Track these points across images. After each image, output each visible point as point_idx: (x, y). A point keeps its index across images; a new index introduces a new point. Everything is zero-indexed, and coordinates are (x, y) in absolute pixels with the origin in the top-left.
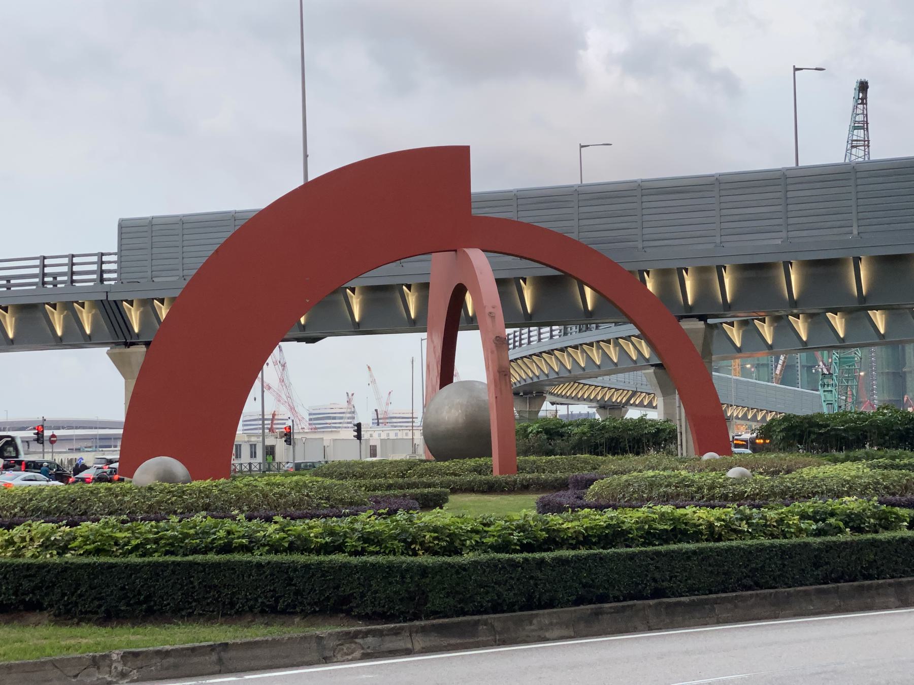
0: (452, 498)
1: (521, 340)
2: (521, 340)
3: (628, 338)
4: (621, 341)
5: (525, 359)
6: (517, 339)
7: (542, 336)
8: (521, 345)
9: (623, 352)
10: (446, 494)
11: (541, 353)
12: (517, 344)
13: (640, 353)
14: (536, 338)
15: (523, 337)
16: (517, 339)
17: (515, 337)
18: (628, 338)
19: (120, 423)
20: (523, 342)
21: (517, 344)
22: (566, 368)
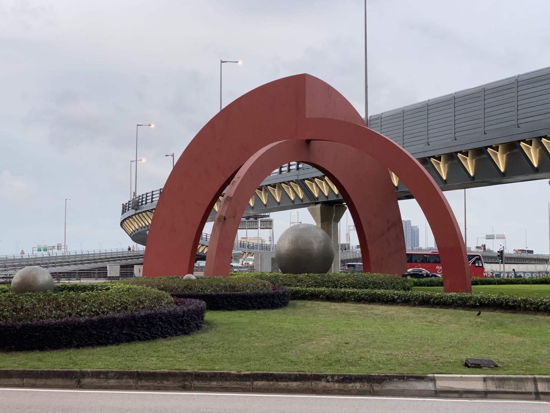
0: (209, 316)
1: (146, 200)
2: (146, 200)
3: (312, 180)
4: (307, 182)
5: (148, 213)
6: (144, 199)
7: (154, 200)
8: (146, 203)
9: (285, 195)
10: (200, 314)
11: (289, 182)
12: (144, 202)
13: (296, 195)
14: (150, 201)
15: (148, 198)
16: (144, 199)
17: (143, 198)
18: (312, 180)
19: (359, 258)
20: (148, 201)
21: (144, 202)
22: (299, 197)
